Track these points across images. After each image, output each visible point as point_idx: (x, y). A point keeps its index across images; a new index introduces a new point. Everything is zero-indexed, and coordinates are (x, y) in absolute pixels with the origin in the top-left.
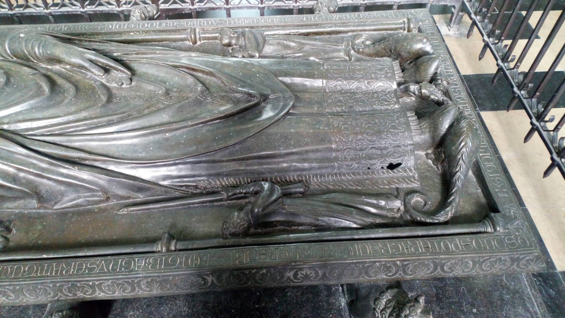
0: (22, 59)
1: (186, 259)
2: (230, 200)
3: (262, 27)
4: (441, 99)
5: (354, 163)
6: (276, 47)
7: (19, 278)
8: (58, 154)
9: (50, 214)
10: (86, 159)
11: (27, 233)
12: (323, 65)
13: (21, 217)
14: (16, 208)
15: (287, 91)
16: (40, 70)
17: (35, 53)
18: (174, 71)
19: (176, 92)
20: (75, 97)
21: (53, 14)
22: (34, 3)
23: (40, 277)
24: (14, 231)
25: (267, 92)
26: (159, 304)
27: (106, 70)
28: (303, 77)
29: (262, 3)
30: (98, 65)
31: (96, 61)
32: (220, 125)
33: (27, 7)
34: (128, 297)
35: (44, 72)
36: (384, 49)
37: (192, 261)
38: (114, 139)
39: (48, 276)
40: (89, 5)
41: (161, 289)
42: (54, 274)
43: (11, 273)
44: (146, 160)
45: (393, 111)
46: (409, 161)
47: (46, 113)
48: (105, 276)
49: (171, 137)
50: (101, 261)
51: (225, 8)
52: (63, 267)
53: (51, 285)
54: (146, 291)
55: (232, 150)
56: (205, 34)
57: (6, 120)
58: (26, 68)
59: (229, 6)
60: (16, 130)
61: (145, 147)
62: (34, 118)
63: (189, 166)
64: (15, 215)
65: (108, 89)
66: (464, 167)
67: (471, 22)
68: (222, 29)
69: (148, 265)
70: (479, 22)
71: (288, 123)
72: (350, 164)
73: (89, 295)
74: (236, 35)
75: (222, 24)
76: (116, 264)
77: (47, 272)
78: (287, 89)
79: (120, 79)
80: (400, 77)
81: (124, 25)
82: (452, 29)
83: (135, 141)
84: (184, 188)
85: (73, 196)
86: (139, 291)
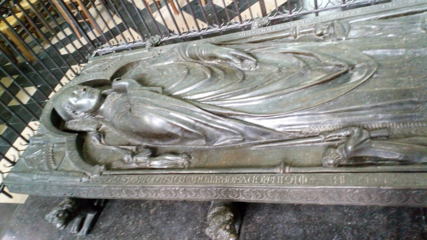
2: (327, 141)
3: (347, 18)
6: (360, 31)
11: (199, 159)
14: (193, 145)
17: (202, 54)
18: (284, 56)
22: (193, 30)
24: (193, 158)
25: (355, 62)
26: (276, 214)
27: (242, 59)
29: (344, 3)
32: (318, 88)
33: (189, 32)
35: (206, 65)
38: (248, 102)
40: (224, 25)
41: (281, 198)
42: (216, 182)
43: (194, 180)
44: (267, 114)
47: (209, 89)
49: (283, 98)
50: (243, 176)
56: (303, 29)
57: (189, 94)
61: (267, 106)
63: (296, 118)
64: (193, 149)
65: (243, 72)
68: (316, 24)
73: (236, 197)
76: (251, 179)
77: (212, 181)
79: (250, 65)
81: (249, 33)
83: (260, 102)
84: (292, 133)
85: (224, 137)
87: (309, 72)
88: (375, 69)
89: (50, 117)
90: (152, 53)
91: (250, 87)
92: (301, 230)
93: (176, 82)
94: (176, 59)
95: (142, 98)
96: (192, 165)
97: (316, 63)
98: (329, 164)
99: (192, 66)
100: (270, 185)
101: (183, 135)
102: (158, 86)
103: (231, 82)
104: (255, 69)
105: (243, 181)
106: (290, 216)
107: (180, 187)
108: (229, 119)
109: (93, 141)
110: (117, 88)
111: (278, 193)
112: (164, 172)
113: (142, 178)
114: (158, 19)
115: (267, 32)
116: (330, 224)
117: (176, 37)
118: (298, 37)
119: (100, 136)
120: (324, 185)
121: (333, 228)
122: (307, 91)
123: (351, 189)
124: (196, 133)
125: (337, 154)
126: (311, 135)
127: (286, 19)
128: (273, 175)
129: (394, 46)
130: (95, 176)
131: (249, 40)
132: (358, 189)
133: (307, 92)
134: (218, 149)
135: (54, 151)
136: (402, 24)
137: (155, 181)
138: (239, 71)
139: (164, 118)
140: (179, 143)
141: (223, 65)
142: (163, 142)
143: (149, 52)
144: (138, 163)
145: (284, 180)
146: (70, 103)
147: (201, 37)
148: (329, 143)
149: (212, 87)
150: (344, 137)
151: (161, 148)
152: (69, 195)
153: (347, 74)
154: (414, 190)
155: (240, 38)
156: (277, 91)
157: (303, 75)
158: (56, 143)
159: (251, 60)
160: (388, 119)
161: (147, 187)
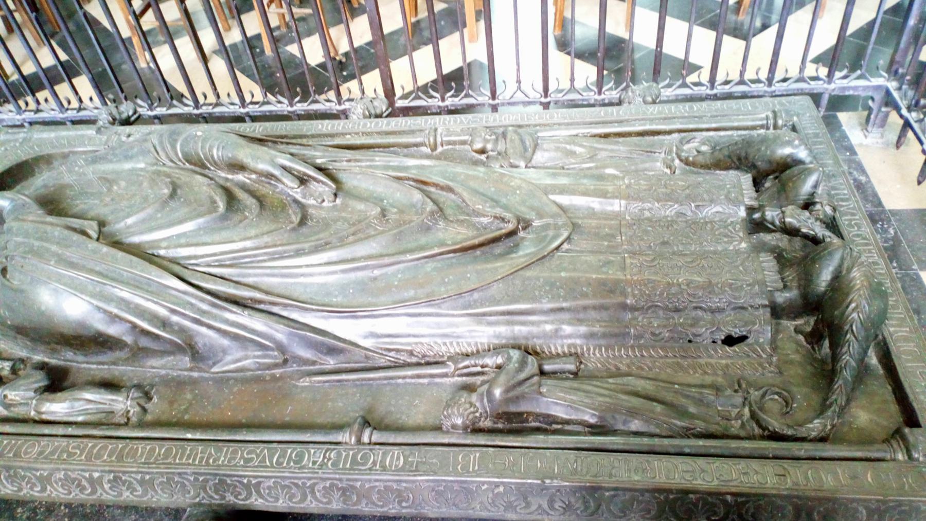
0: (195, 165)
1: (383, 457)
2: (459, 376)
3: (536, 126)
4: (820, 235)
6: (553, 154)
7: (152, 463)
8: (225, 293)
9: (207, 379)
10: (260, 302)
11: (171, 403)
12: (623, 178)
13: (167, 382)
14: (162, 367)
15: (560, 216)
16: (217, 179)
17: (212, 157)
18: (395, 185)
19: (395, 213)
20: (257, 216)
21: (251, 114)
23: (179, 464)
24: (155, 399)
25: (531, 215)
27: (303, 180)
28: (589, 195)
30: (293, 174)
31: (290, 168)
33: (217, 105)
34: (296, 511)
35: (222, 182)
36: (729, 157)
37: (391, 461)
38: (302, 275)
39: (189, 464)
40: (299, 102)
42: (197, 462)
43: (141, 456)
45: (738, 252)
47: (216, 237)
48: (266, 472)
50: (262, 451)
51: (490, 104)
52: (210, 453)
53: (192, 479)
54: (321, 502)
55: (467, 299)
56: (450, 136)
57: (164, 244)
58: (199, 177)
59: (497, 101)
60: (176, 258)
61: (343, 288)
62: (201, 242)
64: (162, 376)
65: (302, 207)
66: (856, 346)
67: (901, 122)
69: (328, 460)
70: (916, 122)
71: (558, 262)
72: (657, 332)
73: (243, 500)
74: (493, 137)
75: (475, 121)
76: (283, 455)
77: (189, 457)
78: (561, 212)
80: (751, 198)
81: (339, 125)
82: (871, 135)
83: (331, 279)
84: (392, 354)
85: (240, 354)
86: (311, 502)
87: (442, 224)
88: (565, 235)
90: (104, 138)
91: (313, 244)
93: (137, 212)
94: (150, 159)
95: (37, 243)
96: (149, 417)
97: (459, 207)
98: (454, 427)
99: (188, 179)
100: (320, 471)
101: (136, 342)
102: (92, 219)
103: (273, 227)
104: (331, 204)
105: (264, 460)
107: (102, 471)
111: (339, 489)
112: (70, 431)
113: (8, 444)
115: (379, 130)
117: (187, 110)
120: (435, 474)
122: (429, 265)
123: (489, 483)
124: (170, 340)
125: (471, 404)
126: (432, 360)
127: (434, 111)
128: (333, 447)
129: (607, 192)
131: (337, 141)
132: (502, 483)
133: (430, 266)
134: (222, 381)
136: (630, 152)
137: (41, 453)
138: (294, 206)
139: (88, 298)
140: (127, 361)
141: (261, 187)
142: (86, 355)
143: (98, 136)
145: (354, 462)
147: (247, 119)
148: (464, 378)
149: (225, 234)
150: (491, 368)
151: (79, 368)
153: (515, 238)
154: (608, 490)
155: (319, 132)
156: (370, 257)
157: (429, 229)
159: (323, 183)
160: (580, 336)
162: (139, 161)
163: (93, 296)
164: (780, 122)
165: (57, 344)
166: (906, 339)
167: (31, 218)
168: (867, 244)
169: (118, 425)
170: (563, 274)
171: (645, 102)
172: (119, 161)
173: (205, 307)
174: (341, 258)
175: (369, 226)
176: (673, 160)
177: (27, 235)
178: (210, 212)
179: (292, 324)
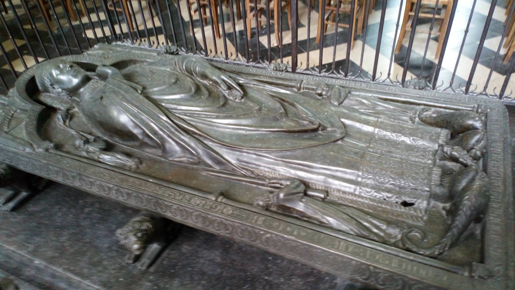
5: (373, 191)
9: (166, 162)
13: (150, 159)
18: (270, 98)
24: (144, 165)
25: (328, 125)
32: (284, 136)
35: (197, 82)
36: (443, 121)
40: (252, 61)
46: (422, 203)
47: (187, 103)
57: (165, 101)
58: (189, 79)
78: (343, 127)
79: (236, 96)
80: (443, 141)
89: (27, 81)
92: (219, 271)
95: (116, 89)
96: (139, 171)
98: (258, 205)
104: (239, 101)
106: (216, 255)
108: (191, 137)
109: (58, 119)
110: (99, 73)
114: (199, 36)
116: (249, 273)
118: (302, 91)
119: (67, 117)
121: (248, 277)
125: (269, 198)
130: (41, 150)
135: (15, 116)
142: (123, 141)
144: (88, 152)
145: (211, 207)
146: (51, 75)
152: (7, 162)
156: (244, 126)
158: (20, 109)
159: (238, 91)
161: (84, 175)
162: (168, 68)
163: (131, 115)
164: (480, 110)
165: (114, 133)
166: (496, 224)
167: (117, 79)
168: (498, 177)
169: (125, 170)
170: (332, 153)
171: (415, 88)
172: (160, 66)
173: (173, 130)
174: (235, 123)
175: (252, 113)
176: (415, 118)
177: (114, 85)
178: (187, 93)
179: (205, 146)
